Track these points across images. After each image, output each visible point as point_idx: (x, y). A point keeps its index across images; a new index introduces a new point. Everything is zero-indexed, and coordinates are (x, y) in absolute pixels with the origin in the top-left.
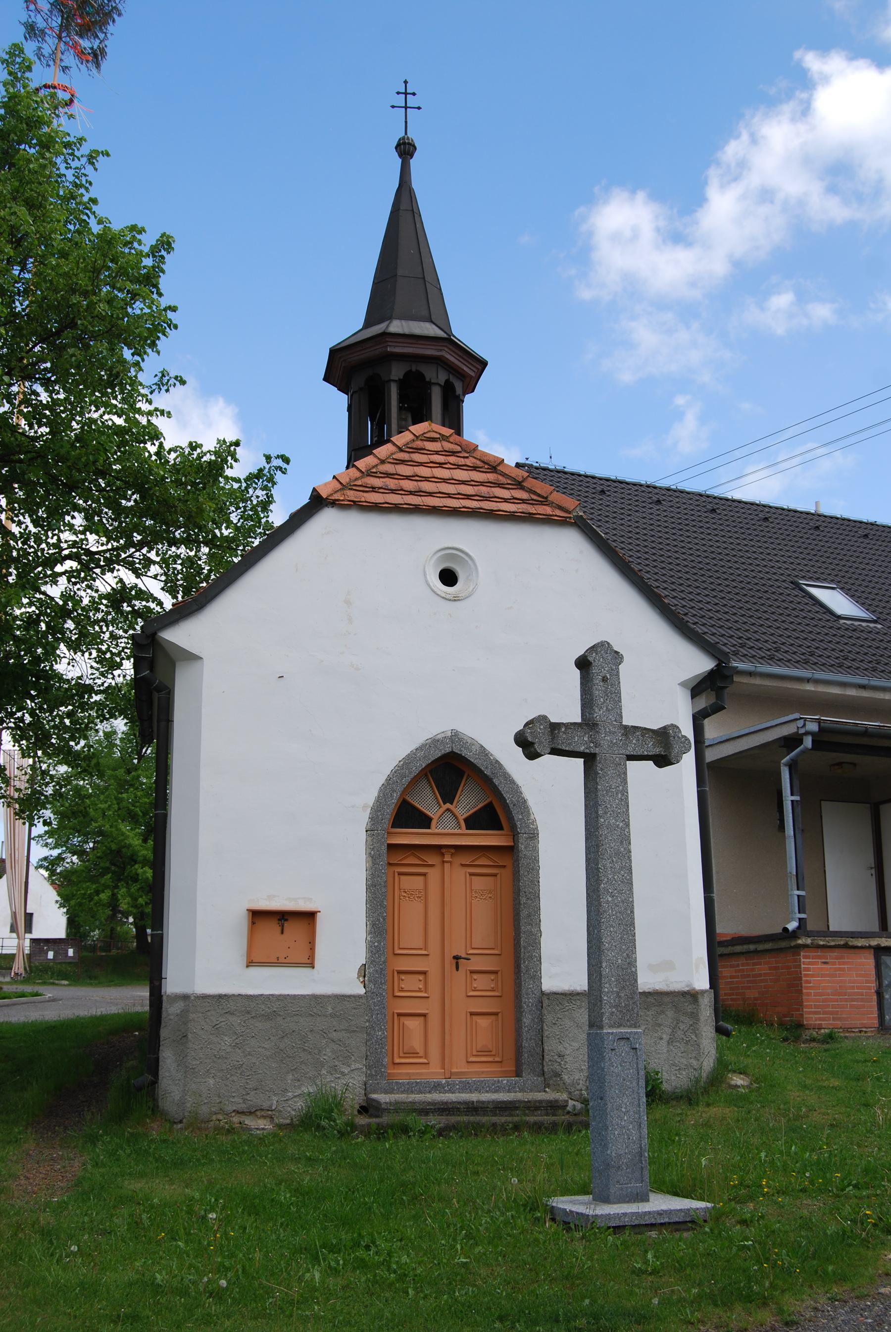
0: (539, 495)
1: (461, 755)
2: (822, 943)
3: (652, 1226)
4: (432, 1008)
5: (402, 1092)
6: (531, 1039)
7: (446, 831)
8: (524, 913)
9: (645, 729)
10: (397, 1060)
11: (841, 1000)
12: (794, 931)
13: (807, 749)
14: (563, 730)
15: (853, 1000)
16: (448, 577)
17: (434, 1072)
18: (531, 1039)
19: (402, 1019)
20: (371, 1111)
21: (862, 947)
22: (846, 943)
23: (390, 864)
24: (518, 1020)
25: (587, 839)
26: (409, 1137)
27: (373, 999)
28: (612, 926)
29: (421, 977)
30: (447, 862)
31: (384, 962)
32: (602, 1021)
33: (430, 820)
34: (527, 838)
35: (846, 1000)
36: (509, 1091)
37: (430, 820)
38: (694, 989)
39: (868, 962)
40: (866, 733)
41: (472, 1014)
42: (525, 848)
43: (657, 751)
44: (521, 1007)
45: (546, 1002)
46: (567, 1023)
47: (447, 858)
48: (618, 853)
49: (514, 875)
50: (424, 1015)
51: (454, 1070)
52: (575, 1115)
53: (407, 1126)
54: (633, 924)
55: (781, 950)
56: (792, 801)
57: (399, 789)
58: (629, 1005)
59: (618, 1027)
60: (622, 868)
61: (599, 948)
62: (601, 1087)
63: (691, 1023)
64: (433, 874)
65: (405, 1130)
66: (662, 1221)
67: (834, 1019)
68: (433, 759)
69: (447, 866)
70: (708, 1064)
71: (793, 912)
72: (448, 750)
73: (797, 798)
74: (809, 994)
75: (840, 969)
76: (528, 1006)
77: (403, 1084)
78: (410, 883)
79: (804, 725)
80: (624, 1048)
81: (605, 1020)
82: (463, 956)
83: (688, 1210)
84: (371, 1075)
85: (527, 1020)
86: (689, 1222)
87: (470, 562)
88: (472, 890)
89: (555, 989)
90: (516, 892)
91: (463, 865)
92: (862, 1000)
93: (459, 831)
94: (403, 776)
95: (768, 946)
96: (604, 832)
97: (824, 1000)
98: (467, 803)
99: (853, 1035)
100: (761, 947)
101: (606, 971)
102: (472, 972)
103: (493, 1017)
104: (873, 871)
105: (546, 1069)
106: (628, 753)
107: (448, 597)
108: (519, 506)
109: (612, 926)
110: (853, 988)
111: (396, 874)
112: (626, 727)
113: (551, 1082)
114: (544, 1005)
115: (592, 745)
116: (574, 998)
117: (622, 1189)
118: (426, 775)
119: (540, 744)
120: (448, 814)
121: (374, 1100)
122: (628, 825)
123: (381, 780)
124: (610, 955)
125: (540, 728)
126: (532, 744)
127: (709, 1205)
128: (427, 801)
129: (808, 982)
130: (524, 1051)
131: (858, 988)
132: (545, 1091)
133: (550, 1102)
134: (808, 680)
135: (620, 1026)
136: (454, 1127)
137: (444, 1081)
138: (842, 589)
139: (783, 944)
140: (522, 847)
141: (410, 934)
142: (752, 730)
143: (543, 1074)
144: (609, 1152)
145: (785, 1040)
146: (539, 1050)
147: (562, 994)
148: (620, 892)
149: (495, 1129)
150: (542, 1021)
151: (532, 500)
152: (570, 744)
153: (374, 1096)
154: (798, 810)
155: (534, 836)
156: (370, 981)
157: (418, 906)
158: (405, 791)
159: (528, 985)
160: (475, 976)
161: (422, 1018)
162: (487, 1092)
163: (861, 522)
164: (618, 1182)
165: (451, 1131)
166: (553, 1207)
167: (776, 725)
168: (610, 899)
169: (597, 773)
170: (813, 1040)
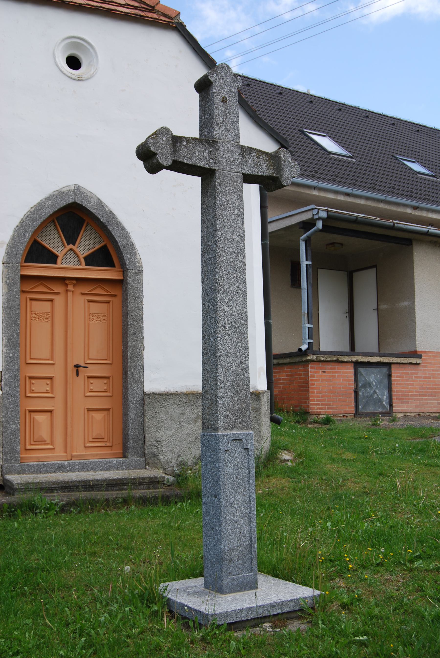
0: (148, 5)
1: (82, 206)
2: (322, 359)
3: (265, 618)
4: (57, 405)
5: (32, 473)
6: (135, 429)
7: (69, 266)
8: (131, 332)
9: (260, 151)
10: (29, 447)
11: (333, 396)
12: (305, 351)
13: (318, 229)
14: (185, 143)
15: (340, 396)
16: (74, 63)
17: (58, 456)
18: (135, 429)
19: (33, 414)
20: (7, 489)
21: (347, 362)
22: (335, 359)
23: (23, 292)
24: (125, 414)
25: (203, 252)
26: (36, 514)
27: (8, 399)
28: (227, 334)
29: (48, 382)
30: (70, 291)
31: (17, 370)
32: (217, 423)
33: (56, 257)
34: (134, 274)
35: (336, 396)
36: (118, 469)
37: (56, 257)
38: (257, 390)
39: (350, 371)
40: (356, 221)
41: (89, 410)
42: (133, 281)
43: (270, 172)
44: (127, 404)
45: (147, 400)
46: (163, 416)
47: (70, 287)
48: (234, 266)
49: (123, 302)
50: (51, 411)
51: (74, 454)
52: (169, 486)
53: (34, 505)
54: (246, 333)
55: (295, 363)
56: (307, 265)
57: (31, 230)
58: (241, 409)
59: (232, 429)
60: (237, 280)
61: (215, 355)
62: (215, 486)
63: (255, 415)
64: (59, 300)
65: (32, 508)
66: (275, 613)
67: (328, 408)
68: (59, 207)
69: (70, 294)
70: (266, 445)
71: (305, 338)
72: (71, 201)
73: (310, 263)
74: (313, 392)
75: (333, 376)
76: (133, 403)
77: (33, 466)
78: (38, 307)
79: (318, 213)
80: (237, 448)
81: (220, 423)
82: (83, 364)
83: (298, 600)
84: (7, 460)
85: (132, 414)
86: (299, 610)
87: (92, 50)
88: (89, 314)
89: (154, 391)
90: (125, 316)
91: (83, 294)
92: (346, 396)
93: (80, 267)
94: (34, 220)
95: (287, 360)
96: (221, 244)
97: (323, 396)
98: (86, 245)
99: (339, 418)
100: (281, 361)
101: (221, 377)
102: (89, 377)
103: (106, 412)
104: (347, 315)
105: (146, 452)
106: (244, 172)
107: (73, 77)
108: (132, 10)
109: (227, 334)
110: (340, 388)
111: (28, 300)
112: (243, 147)
113: (150, 461)
114: (146, 403)
115: (211, 161)
116: (169, 397)
117: (234, 579)
118: (53, 221)
119: (162, 155)
120: (71, 253)
121: (8, 481)
122: (243, 239)
123: (16, 222)
124: (226, 361)
125: (163, 140)
126: (155, 154)
127: (317, 592)
128: (54, 242)
129: (313, 384)
130: (130, 439)
131: (343, 388)
132: (146, 468)
133: (151, 478)
134: (315, 188)
135: (233, 428)
136: (74, 504)
137: (66, 463)
138: (330, 137)
139: (297, 359)
140: (130, 280)
141: (40, 347)
142: (280, 217)
143: (144, 455)
144: (222, 546)
145: (298, 422)
146: (141, 437)
147: (159, 394)
148: (236, 302)
149: (108, 504)
150: (143, 415)
151: (143, 8)
152: (191, 158)
153: (9, 477)
154: (310, 271)
155: (139, 272)
156: (5, 385)
157: (47, 325)
158: (36, 232)
159: (133, 387)
160: (92, 381)
161: (49, 414)
162: (101, 470)
163: (336, 102)
164: (230, 573)
165: (71, 506)
166: (169, 599)
167: (298, 214)
168: (226, 309)
169: (215, 189)
170: (315, 422)
